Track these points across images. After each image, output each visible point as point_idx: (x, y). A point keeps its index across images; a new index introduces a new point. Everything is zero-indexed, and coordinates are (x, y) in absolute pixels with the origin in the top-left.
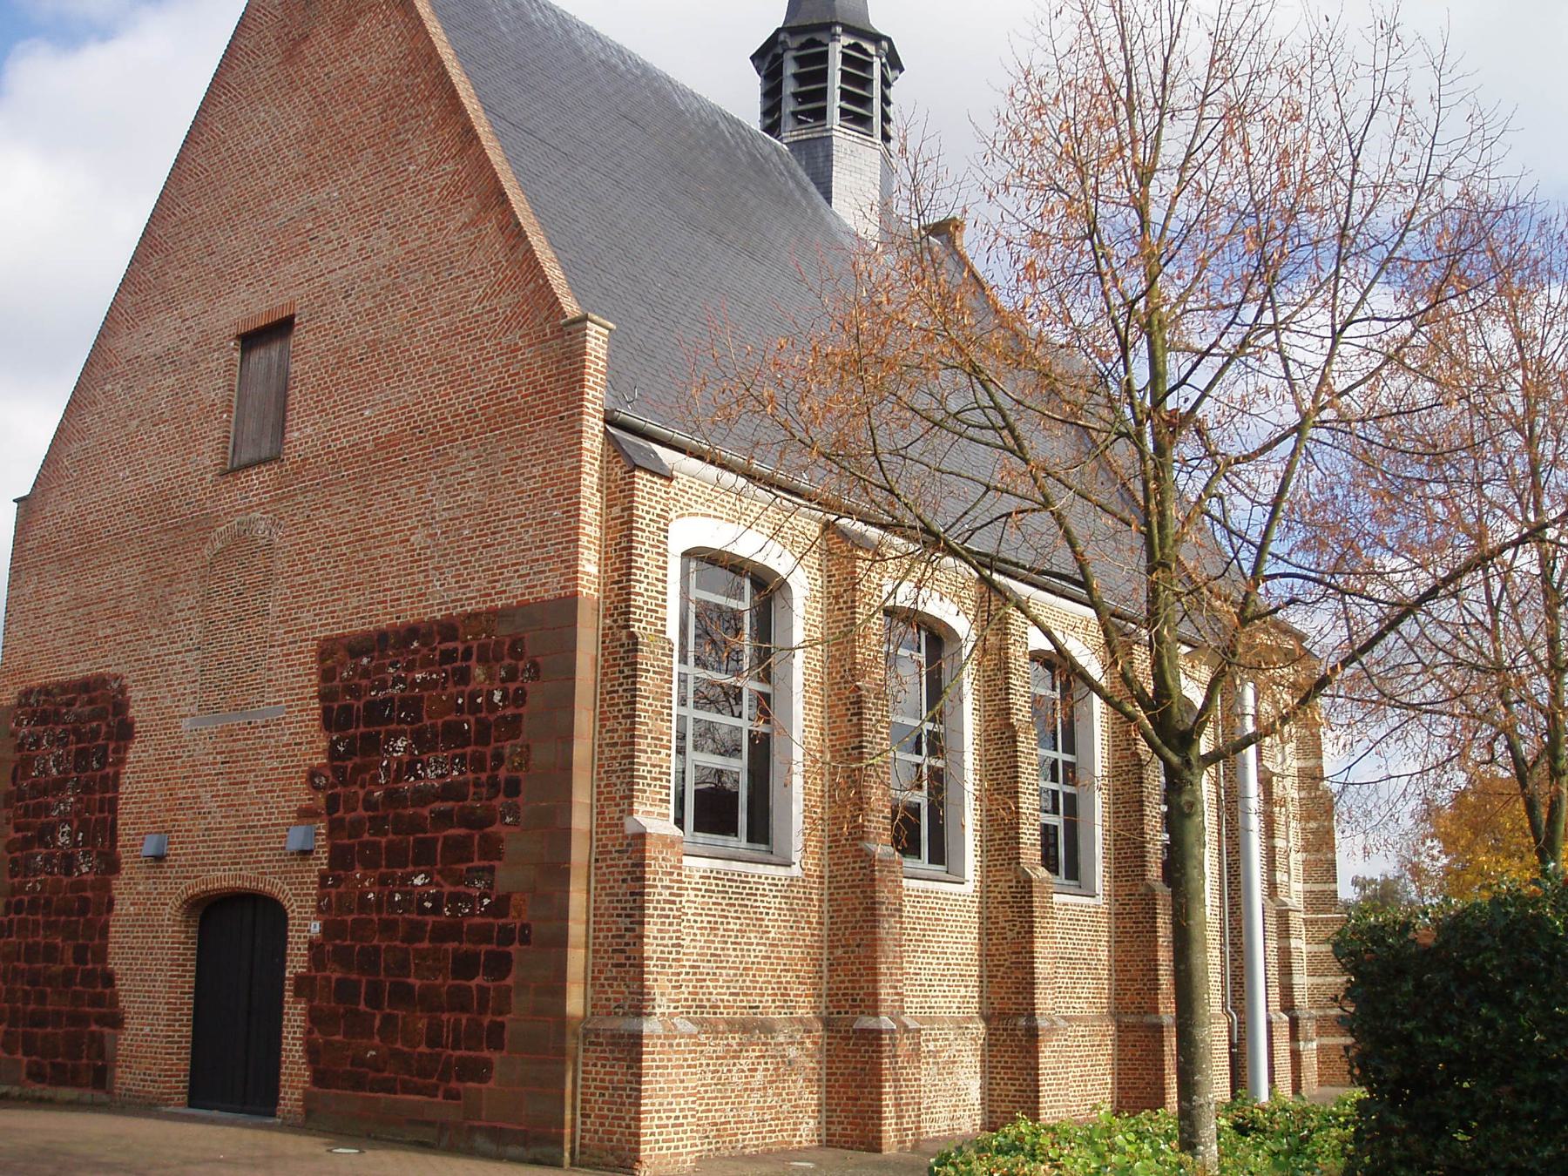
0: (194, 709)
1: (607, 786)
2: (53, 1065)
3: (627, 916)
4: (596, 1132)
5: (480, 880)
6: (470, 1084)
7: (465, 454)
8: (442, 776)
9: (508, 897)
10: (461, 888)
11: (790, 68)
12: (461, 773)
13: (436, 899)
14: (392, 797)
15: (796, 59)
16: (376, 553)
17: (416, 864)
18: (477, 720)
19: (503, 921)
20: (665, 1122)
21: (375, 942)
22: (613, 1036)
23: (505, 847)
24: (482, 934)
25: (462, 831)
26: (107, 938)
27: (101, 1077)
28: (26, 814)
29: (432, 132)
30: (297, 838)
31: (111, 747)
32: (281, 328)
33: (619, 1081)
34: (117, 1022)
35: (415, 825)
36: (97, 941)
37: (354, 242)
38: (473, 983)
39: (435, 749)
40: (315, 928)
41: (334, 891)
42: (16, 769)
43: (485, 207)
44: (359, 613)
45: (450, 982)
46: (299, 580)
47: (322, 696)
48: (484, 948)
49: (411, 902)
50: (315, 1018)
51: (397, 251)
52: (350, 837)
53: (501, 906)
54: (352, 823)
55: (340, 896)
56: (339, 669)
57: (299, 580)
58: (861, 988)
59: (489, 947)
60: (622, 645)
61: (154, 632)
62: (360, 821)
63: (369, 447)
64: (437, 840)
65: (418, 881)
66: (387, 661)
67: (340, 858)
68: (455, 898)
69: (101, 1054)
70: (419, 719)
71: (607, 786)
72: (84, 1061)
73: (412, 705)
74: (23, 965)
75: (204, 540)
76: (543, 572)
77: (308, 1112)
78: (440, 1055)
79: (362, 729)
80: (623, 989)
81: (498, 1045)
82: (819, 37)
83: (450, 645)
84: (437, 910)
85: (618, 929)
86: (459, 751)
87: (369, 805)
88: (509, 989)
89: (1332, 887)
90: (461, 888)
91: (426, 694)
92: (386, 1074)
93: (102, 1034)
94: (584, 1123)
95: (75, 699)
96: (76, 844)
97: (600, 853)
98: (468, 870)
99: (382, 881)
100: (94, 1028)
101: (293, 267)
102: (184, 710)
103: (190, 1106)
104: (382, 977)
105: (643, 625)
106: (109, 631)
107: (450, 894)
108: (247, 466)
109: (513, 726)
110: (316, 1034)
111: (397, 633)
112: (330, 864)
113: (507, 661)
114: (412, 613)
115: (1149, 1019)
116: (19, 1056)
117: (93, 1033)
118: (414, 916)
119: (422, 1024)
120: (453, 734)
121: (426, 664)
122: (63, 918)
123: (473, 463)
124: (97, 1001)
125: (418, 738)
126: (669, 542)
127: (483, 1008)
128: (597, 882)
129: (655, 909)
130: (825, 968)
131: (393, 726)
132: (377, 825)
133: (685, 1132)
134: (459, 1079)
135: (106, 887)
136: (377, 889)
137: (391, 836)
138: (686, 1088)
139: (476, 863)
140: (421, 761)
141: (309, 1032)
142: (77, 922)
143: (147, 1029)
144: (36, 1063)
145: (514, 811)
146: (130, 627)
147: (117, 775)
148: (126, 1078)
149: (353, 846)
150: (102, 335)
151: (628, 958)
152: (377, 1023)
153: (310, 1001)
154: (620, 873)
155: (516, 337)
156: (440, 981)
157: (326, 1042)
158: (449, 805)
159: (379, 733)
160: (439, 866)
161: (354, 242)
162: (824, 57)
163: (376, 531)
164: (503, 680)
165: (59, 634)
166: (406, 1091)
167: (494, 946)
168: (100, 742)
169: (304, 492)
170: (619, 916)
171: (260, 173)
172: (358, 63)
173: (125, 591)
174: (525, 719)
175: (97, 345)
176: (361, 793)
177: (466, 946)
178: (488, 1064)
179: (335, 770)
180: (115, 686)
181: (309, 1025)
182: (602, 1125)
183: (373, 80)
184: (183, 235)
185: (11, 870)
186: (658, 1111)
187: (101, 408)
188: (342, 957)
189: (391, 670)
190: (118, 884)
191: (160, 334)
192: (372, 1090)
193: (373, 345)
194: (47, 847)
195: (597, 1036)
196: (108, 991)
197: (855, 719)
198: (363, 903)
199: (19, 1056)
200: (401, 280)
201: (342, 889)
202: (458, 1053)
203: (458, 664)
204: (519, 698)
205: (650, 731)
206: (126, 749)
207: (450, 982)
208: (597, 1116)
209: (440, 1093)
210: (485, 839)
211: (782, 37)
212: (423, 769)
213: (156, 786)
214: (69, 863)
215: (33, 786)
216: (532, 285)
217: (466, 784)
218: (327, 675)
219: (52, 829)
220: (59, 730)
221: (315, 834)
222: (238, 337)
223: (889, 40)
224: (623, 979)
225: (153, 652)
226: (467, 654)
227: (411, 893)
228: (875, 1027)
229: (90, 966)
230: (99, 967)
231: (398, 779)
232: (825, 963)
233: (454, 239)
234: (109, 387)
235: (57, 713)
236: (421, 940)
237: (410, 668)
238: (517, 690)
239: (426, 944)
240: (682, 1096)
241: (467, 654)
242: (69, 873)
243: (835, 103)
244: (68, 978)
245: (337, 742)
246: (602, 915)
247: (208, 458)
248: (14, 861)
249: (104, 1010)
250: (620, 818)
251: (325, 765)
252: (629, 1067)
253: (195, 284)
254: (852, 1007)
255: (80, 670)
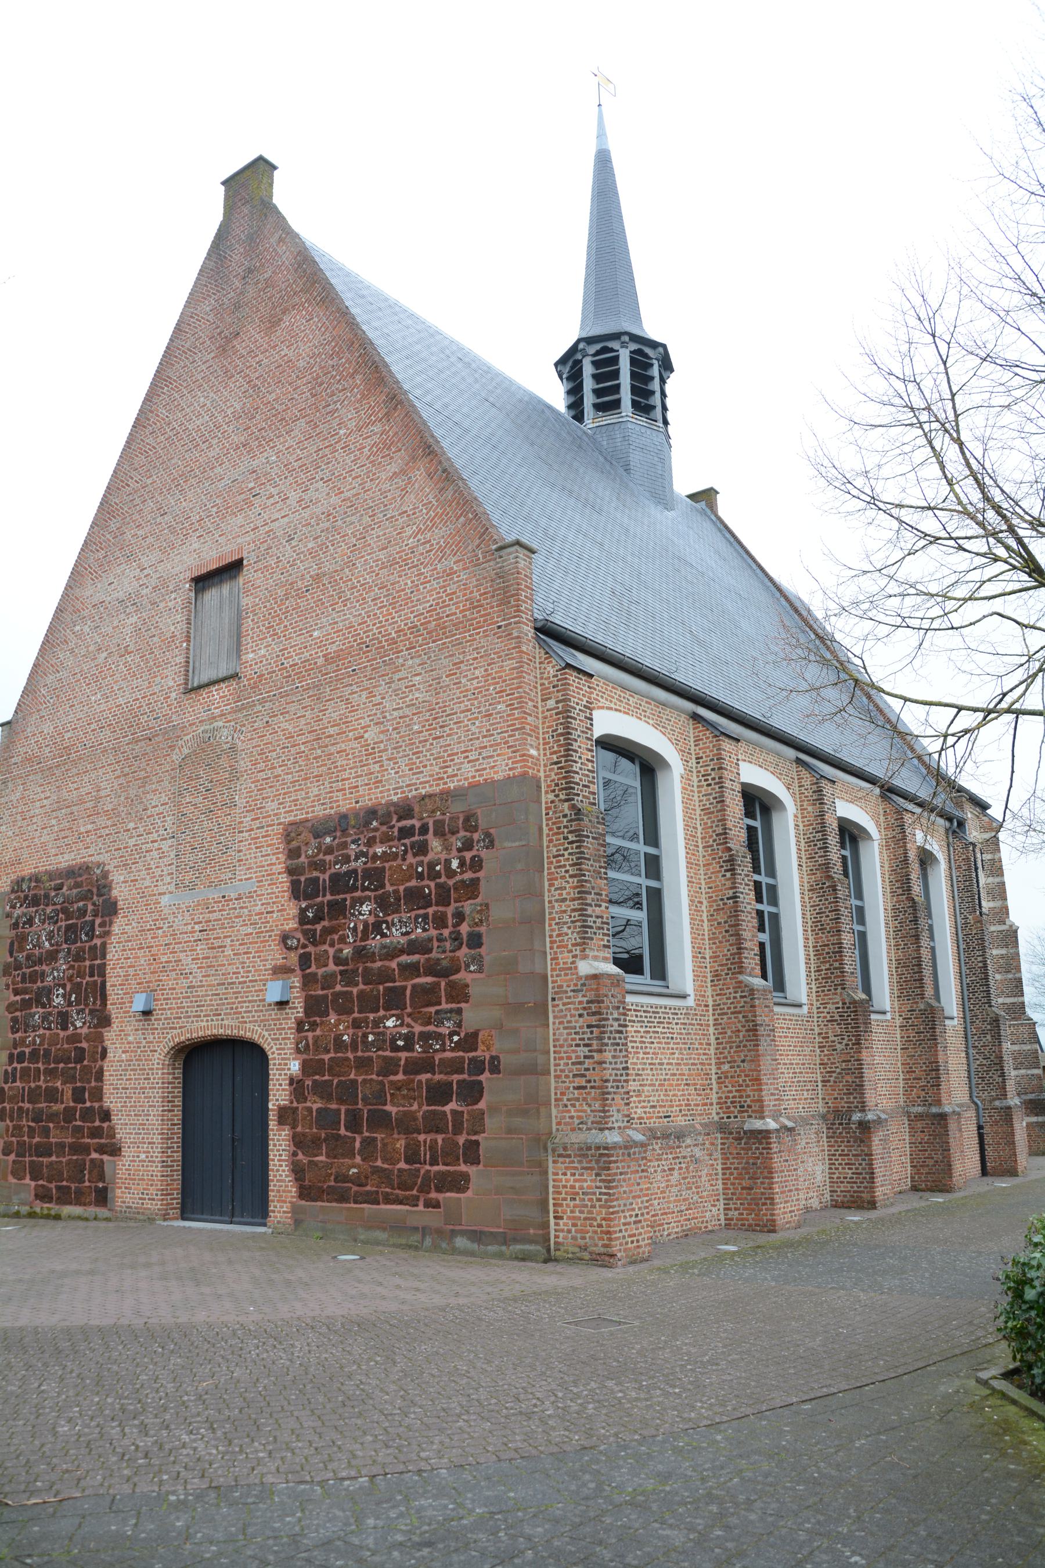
0: (172, 888)
1: (559, 935)
2: (58, 1188)
3: (585, 1045)
4: (569, 1231)
5: (449, 1019)
6: (448, 1194)
7: (410, 662)
8: (407, 933)
9: (475, 1035)
10: (431, 1028)
11: (588, 370)
12: (425, 930)
13: (409, 1039)
14: (361, 954)
15: (593, 363)
16: (333, 749)
17: (386, 1009)
18: (437, 885)
19: (473, 1054)
20: (628, 1220)
21: (352, 1076)
22: (581, 1149)
23: (472, 991)
24: (455, 1066)
25: (429, 979)
26: (102, 1081)
27: (102, 1197)
28: (23, 980)
29: (359, 401)
30: (274, 991)
31: (98, 921)
32: (234, 568)
33: (588, 1187)
34: (115, 1151)
35: (385, 976)
36: (93, 1084)
37: (293, 496)
38: (447, 1108)
39: (397, 911)
40: (295, 1067)
41: (310, 1034)
42: (12, 944)
43: (413, 459)
44: (318, 801)
45: (425, 1108)
46: (263, 775)
47: (291, 871)
48: (456, 1077)
49: (384, 1041)
50: (298, 1142)
51: (334, 500)
52: (323, 989)
53: (470, 1041)
54: (325, 977)
55: (316, 1039)
56: (303, 848)
57: (263, 775)
58: (748, 1096)
59: (461, 1077)
60: (565, 816)
61: (131, 825)
62: (333, 975)
63: (321, 661)
64: (405, 988)
65: (390, 1023)
66: (349, 839)
67: (315, 1008)
68: (425, 1037)
69: (102, 1177)
70: (383, 886)
71: (559, 935)
72: (87, 1184)
73: (375, 876)
74: (26, 1105)
75: (172, 747)
76: (491, 757)
77: (297, 1223)
78: (418, 1170)
79: (329, 897)
80: (585, 1107)
81: (476, 1161)
82: (612, 344)
83: (407, 823)
84: (409, 1047)
85: (577, 1057)
86: (422, 912)
87: (338, 961)
88: (482, 1113)
89: (1020, 999)
90: (431, 1028)
91: (387, 865)
92: (368, 1188)
93: (102, 1160)
94: (557, 1224)
95: (62, 885)
96: (70, 1004)
97: (556, 993)
98: (437, 1012)
99: (356, 1024)
100: (94, 1155)
101: (240, 519)
102: (162, 889)
103: (183, 1219)
104: (360, 1106)
105: (580, 798)
106: (90, 827)
107: (421, 1033)
108: (208, 685)
109: (471, 889)
110: (300, 1156)
111: (356, 815)
112: (306, 1012)
113: (462, 833)
114: (371, 797)
115: (934, 1110)
116: (27, 1181)
117: (92, 1160)
118: (388, 1053)
119: (401, 1144)
120: (416, 898)
121: (386, 839)
122: (62, 1065)
123: (419, 669)
124: (96, 1133)
125: (384, 903)
126: (594, 728)
127: (458, 1129)
128: (555, 1017)
129: (609, 1038)
130: (714, 1082)
131: (358, 894)
132: (348, 977)
133: (643, 1227)
134: (439, 1190)
135: (100, 1038)
136: (351, 1031)
137: (361, 986)
138: (641, 1190)
139: (444, 1006)
140: (386, 922)
141: (295, 1154)
142: (75, 1068)
143: (143, 1156)
144: (42, 1186)
145: (478, 960)
146: (109, 823)
147: (104, 945)
148: (124, 1196)
149: (326, 996)
150: (69, 587)
151: (589, 1081)
152: (357, 1145)
153: (294, 1127)
154: (577, 1009)
155: (450, 562)
156: (415, 1107)
157: (310, 1162)
158: (416, 958)
159: (345, 900)
160: (409, 1010)
161: (293, 496)
162: (615, 360)
163: (332, 731)
164: (459, 850)
165: (45, 831)
166: (388, 1201)
167: (465, 1076)
168: (87, 918)
169: (262, 702)
170: (578, 1045)
171: (204, 446)
172: (286, 351)
173: (103, 793)
174: (482, 883)
175: (65, 596)
176: (331, 951)
177: (438, 1077)
178: (466, 1177)
179: (305, 933)
180: (98, 872)
181: (293, 1148)
182: (574, 1225)
183: (301, 364)
184: (137, 501)
185: (12, 1028)
186: (623, 1211)
187: (72, 645)
188: (322, 1090)
189: (353, 846)
190: (110, 1036)
191: (124, 580)
192: (356, 1202)
193: (317, 578)
194: (44, 1006)
195: (565, 1149)
196: (105, 1125)
197: (728, 874)
198: (339, 1044)
199: (27, 1181)
200: (340, 523)
201: (318, 1032)
202: (436, 1168)
203: (416, 838)
204: (476, 864)
205: (593, 888)
206: (111, 923)
207: (425, 1108)
208: (569, 1218)
209: (421, 1203)
210: (451, 985)
211: (581, 346)
212: (388, 928)
213: (141, 953)
214: (64, 1020)
215: (28, 958)
216: (462, 519)
217: (430, 940)
218: (293, 853)
219: (49, 991)
220: (49, 910)
221: (291, 989)
222: (193, 580)
223: (664, 346)
224: (585, 1099)
225: (132, 842)
226: (424, 830)
227: (383, 1034)
228: (764, 1128)
229: (88, 1104)
230: (96, 1105)
231: (365, 937)
232: (714, 1077)
233: (386, 486)
234: (78, 628)
235: (47, 896)
236: (396, 1073)
237: (371, 842)
238: (473, 858)
239: (400, 1077)
240: (639, 1197)
241: (424, 830)
242: (65, 1028)
243: (626, 395)
244: (69, 1114)
245: (306, 909)
246: (561, 1046)
247: (171, 680)
248: (15, 1020)
249: (103, 1141)
250: (573, 963)
251: (296, 929)
252: (597, 1175)
253: (150, 540)
254: (740, 1112)
255: (66, 860)
